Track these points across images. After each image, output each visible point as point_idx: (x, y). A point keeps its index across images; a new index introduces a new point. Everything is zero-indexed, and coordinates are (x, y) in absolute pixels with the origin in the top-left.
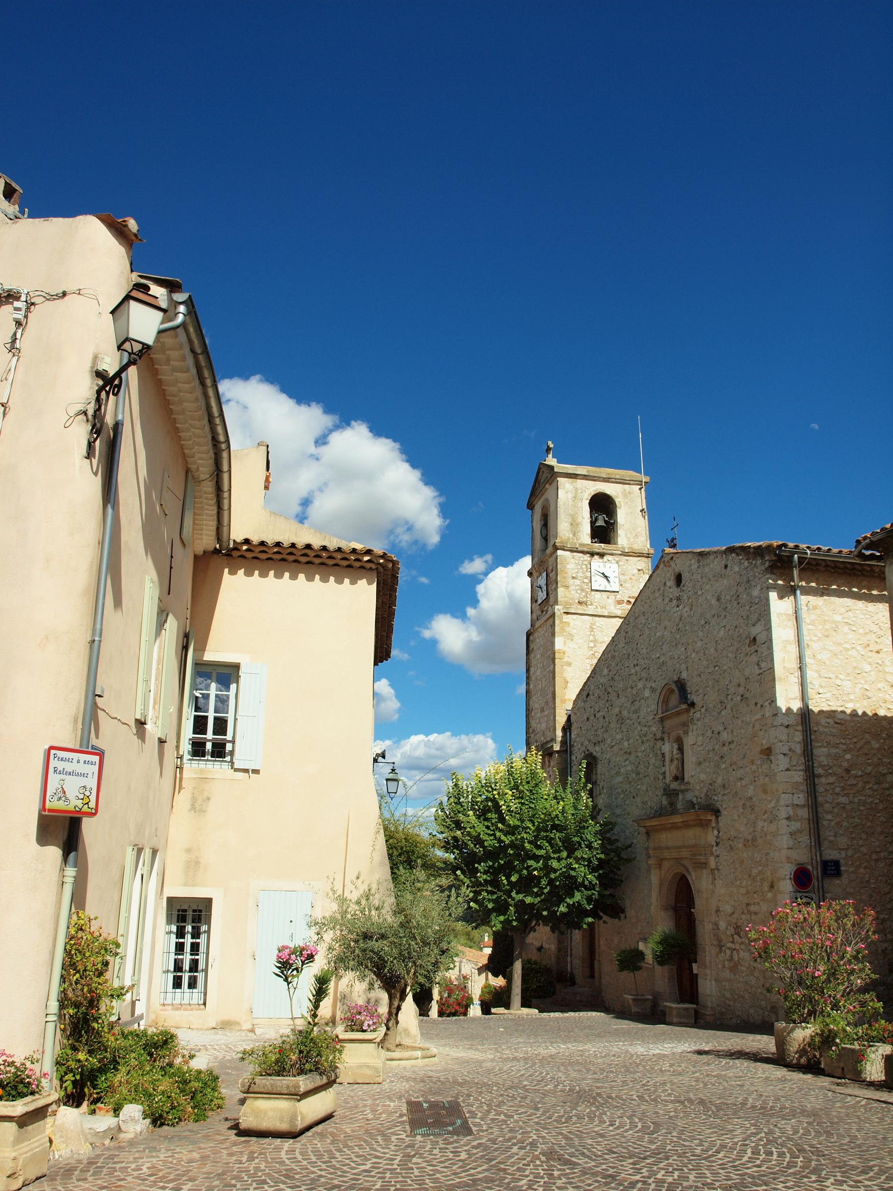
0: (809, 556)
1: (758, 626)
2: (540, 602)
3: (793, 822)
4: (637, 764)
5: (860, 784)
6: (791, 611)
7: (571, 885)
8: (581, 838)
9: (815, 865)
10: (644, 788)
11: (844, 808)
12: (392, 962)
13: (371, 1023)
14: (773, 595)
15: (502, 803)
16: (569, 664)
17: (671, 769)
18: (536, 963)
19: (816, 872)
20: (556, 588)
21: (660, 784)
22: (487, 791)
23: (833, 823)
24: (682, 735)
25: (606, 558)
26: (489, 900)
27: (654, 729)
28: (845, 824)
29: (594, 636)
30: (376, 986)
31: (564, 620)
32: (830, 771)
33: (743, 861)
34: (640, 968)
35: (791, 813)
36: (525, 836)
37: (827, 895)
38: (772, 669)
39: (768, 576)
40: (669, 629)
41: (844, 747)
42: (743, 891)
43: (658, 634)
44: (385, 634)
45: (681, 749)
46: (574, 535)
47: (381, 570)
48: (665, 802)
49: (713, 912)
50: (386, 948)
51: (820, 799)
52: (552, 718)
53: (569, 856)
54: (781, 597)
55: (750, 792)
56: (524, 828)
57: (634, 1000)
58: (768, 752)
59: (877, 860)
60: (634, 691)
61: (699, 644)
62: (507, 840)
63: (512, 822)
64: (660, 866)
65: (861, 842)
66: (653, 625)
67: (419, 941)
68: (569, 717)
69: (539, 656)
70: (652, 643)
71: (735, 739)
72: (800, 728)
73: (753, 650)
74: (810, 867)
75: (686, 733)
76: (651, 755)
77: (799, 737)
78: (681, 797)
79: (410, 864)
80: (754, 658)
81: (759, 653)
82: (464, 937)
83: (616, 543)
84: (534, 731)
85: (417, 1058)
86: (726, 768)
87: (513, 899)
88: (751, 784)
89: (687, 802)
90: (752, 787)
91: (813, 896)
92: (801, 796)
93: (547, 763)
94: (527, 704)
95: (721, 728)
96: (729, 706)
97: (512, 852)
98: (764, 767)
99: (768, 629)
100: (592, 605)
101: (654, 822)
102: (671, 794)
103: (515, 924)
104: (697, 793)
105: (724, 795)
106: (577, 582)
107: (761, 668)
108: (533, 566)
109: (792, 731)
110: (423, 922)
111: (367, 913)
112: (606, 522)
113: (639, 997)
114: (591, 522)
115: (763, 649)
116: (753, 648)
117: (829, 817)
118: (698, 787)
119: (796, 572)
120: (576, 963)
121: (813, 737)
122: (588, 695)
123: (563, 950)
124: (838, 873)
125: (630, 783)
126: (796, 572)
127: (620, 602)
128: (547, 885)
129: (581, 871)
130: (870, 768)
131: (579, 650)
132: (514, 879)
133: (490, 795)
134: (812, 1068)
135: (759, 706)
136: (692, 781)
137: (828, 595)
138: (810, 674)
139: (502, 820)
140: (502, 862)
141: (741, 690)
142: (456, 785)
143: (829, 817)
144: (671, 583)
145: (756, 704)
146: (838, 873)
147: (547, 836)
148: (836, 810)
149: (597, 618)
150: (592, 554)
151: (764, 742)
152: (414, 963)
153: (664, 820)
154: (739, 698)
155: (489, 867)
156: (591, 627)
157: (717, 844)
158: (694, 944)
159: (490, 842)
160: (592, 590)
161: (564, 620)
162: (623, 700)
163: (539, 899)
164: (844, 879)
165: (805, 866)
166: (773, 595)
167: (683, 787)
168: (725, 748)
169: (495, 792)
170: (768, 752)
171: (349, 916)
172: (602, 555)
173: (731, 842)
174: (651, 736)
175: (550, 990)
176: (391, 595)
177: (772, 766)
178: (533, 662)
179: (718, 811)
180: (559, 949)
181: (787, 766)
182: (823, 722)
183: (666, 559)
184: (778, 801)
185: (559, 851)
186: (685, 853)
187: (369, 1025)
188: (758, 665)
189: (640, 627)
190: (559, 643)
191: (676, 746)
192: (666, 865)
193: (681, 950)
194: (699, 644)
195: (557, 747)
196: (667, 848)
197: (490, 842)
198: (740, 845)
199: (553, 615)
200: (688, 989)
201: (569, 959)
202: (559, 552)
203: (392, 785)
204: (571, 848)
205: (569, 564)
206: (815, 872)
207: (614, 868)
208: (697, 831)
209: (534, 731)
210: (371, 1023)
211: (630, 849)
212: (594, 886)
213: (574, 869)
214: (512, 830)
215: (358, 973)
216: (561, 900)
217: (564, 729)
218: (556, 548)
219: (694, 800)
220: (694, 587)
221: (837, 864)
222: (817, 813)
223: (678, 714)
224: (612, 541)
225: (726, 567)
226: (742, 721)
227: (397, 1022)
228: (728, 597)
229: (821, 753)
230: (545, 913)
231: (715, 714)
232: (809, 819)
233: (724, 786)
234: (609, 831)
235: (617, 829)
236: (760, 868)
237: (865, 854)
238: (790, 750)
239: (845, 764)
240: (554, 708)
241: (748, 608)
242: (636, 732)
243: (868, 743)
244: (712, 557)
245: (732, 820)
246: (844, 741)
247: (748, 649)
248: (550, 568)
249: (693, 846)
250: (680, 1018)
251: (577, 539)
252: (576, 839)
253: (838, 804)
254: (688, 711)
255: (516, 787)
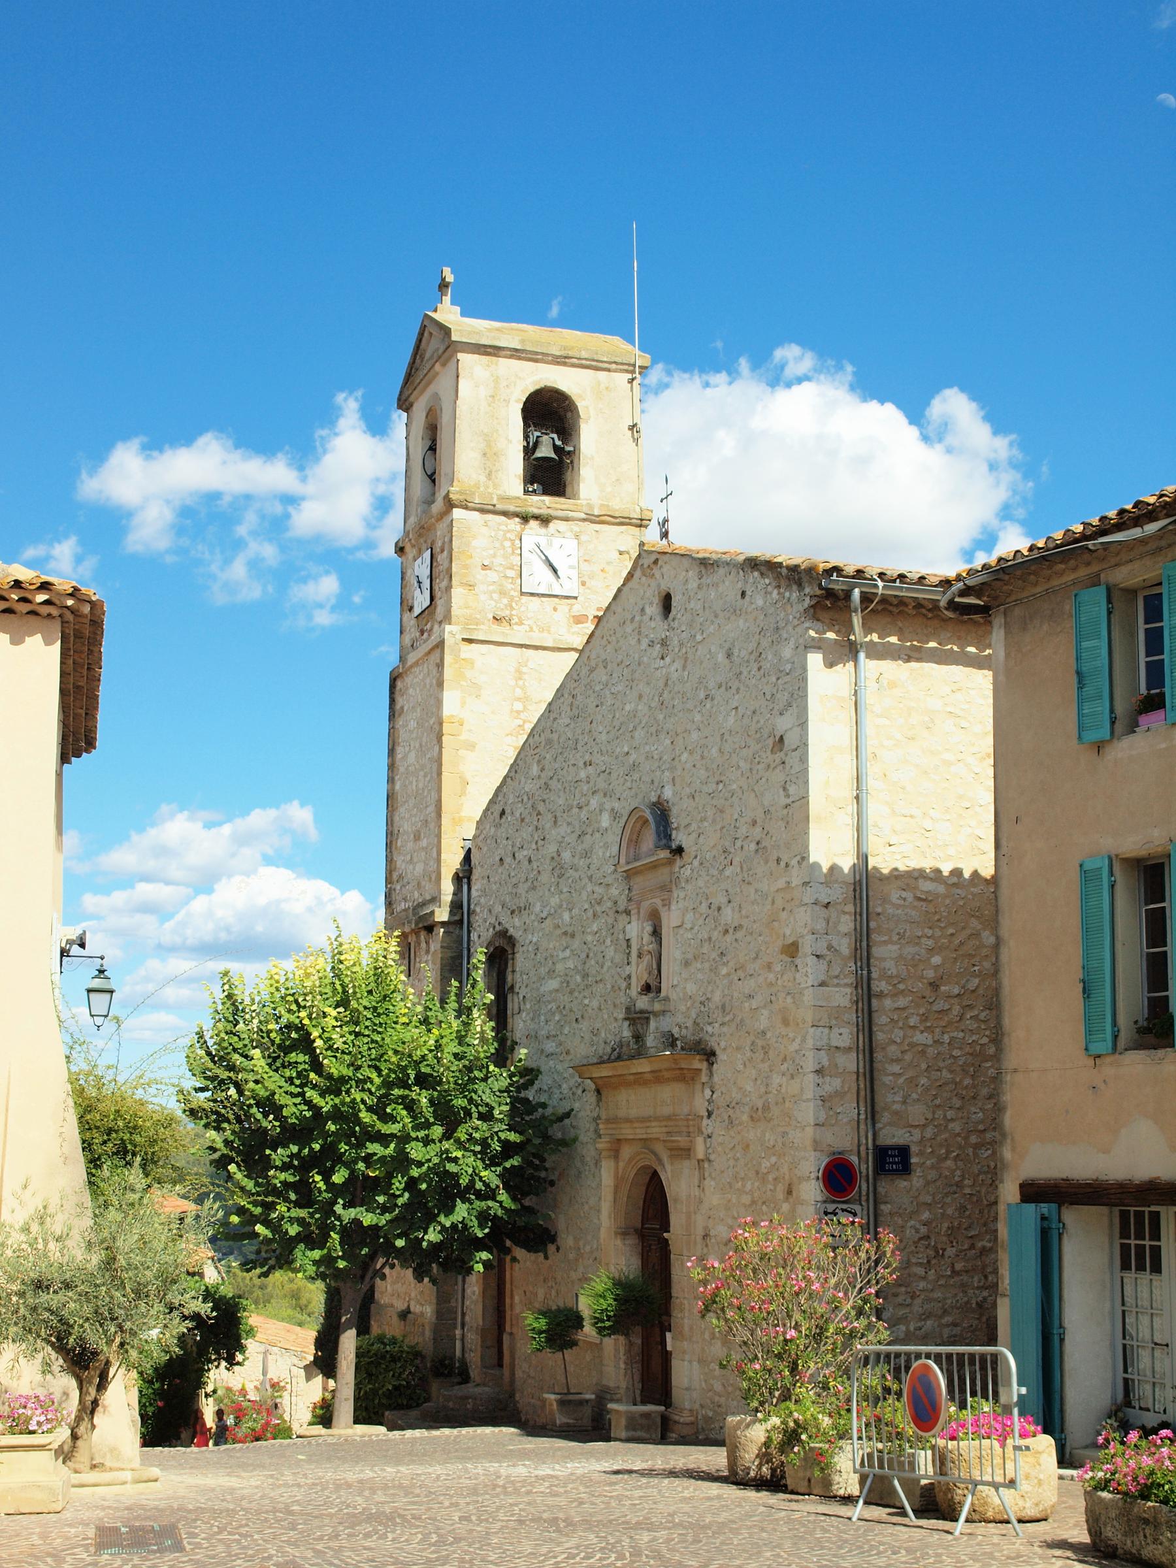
0: (880, 591)
1: (788, 714)
2: (417, 610)
3: (828, 1079)
4: (583, 956)
5: (956, 1010)
6: (846, 691)
7: (448, 1190)
8: (471, 1101)
9: (863, 1154)
10: (595, 1004)
11: (923, 1052)
12: (82, 1326)
13: (43, 1418)
14: (815, 660)
15: (315, 1034)
16: (471, 746)
17: (639, 972)
18: (394, 1341)
19: (864, 1166)
20: (449, 588)
21: (623, 999)
22: (289, 1011)
23: (901, 1080)
24: (660, 908)
25: (554, 525)
26: (291, 1220)
27: (614, 892)
28: (923, 1081)
29: (523, 688)
30: (56, 1368)
31: (463, 656)
32: (901, 986)
33: (748, 1146)
34: (573, 1344)
35: (825, 1062)
36: (358, 1096)
37: (883, 1207)
38: (804, 798)
39: (807, 624)
40: (645, 700)
41: (930, 943)
42: (746, 1199)
43: (628, 707)
44: (83, 712)
45: (656, 933)
46: (489, 476)
47: (69, 617)
48: (627, 1034)
49: (699, 1239)
50: (72, 1305)
51: (880, 1037)
52: (435, 855)
53: (447, 1136)
54: (830, 664)
55: (763, 1022)
56: (358, 1082)
57: (562, 1403)
58: (792, 950)
59: (977, 1147)
60: (584, 815)
61: (695, 735)
62: (326, 1104)
63: (334, 1067)
64: (615, 1154)
65: (950, 1114)
66: (620, 688)
67: (128, 1290)
68: (467, 858)
69: (413, 724)
70: (617, 723)
71: (744, 922)
72: (850, 908)
73: (778, 761)
74: (854, 1159)
75: (667, 903)
76: (608, 942)
77: (847, 924)
78: (653, 1024)
79: (123, 1152)
80: (778, 776)
81: (788, 766)
82: (285, 1302)
83: (575, 496)
84: (401, 877)
85: (124, 1483)
86: (728, 974)
87: (339, 1218)
88: (765, 1007)
89: (663, 1034)
90: (765, 1012)
91: (857, 1208)
92: (845, 1031)
93: (423, 945)
94: (390, 822)
95: (724, 900)
96: (736, 861)
97: (333, 1128)
98: (785, 977)
99: (803, 724)
100: (521, 623)
101: (605, 1071)
102: (638, 1019)
103: (341, 1264)
104: (680, 1019)
105: (723, 1024)
106: (492, 576)
107: (788, 796)
108: (406, 533)
109: (834, 915)
110: (137, 1259)
111: (40, 1246)
112: (556, 449)
113: (571, 1397)
114: (526, 449)
115: (793, 760)
116: (779, 756)
117: (896, 1068)
118: (683, 1008)
119: (857, 620)
120: (469, 1343)
121: (873, 924)
122: (503, 813)
123: (446, 1315)
124: (905, 1168)
125: (571, 993)
126: (857, 620)
127: (579, 619)
128: (404, 1190)
129: (467, 1165)
130: (977, 981)
131: (490, 714)
132: (338, 1178)
133: (292, 1018)
134: (774, 1484)
135: (783, 864)
136: (673, 996)
137: (919, 660)
138: (874, 809)
139: (317, 1066)
140: (317, 1147)
141: (757, 832)
142: (229, 997)
143: (896, 1068)
144: (654, 609)
145: (778, 860)
146: (905, 1168)
147: (404, 1097)
148: (908, 1057)
149: (531, 652)
150: (525, 519)
151: (788, 932)
152: (120, 1327)
153: (621, 1068)
154: (753, 846)
155: (292, 1156)
156: (519, 671)
157: (710, 1115)
158: (668, 1297)
159: (292, 1109)
160: (522, 593)
161: (463, 656)
162: (563, 829)
163: (388, 1216)
164: (917, 1179)
165: (846, 1156)
166: (815, 660)
167: (657, 1007)
168: (729, 938)
169: (303, 1014)
170: (792, 950)
171: (9, 1253)
172: (545, 520)
173: (731, 1112)
174: (609, 904)
175: (402, 1388)
176: (90, 652)
177: (798, 975)
178: (402, 735)
179: (713, 1054)
180: (439, 1314)
181: (822, 977)
182: (894, 896)
183: (647, 561)
184: (804, 1040)
185: (427, 1125)
186: (656, 1130)
187: (39, 1424)
188: (785, 789)
189: (597, 688)
190: (452, 703)
191: (649, 928)
192: (626, 1152)
193: (645, 1308)
194: (695, 735)
195: (442, 914)
196: (628, 1120)
197: (292, 1109)
198: (745, 1118)
199: (440, 645)
200: (655, 1380)
201: (458, 1332)
202: (457, 513)
203: (100, 1000)
204: (450, 1119)
205: (475, 537)
206: (863, 1167)
207: (537, 1153)
208: (678, 1089)
209: (401, 877)
210: (43, 1418)
211: (567, 1121)
212: (493, 1191)
213: (455, 1160)
214: (335, 1086)
215: (24, 1346)
216: (431, 1218)
217: (458, 879)
218: (450, 505)
219: (676, 1031)
220: (690, 625)
221: (904, 1152)
222: (872, 1061)
223: (654, 866)
224: (568, 490)
225: (743, 594)
226: (756, 891)
227: (93, 1427)
228: (744, 653)
229: (886, 953)
230: (400, 1243)
231: (715, 873)
232: (858, 1073)
233: (723, 1007)
234: (525, 1086)
235: (544, 1081)
236: (773, 1159)
237: (958, 1135)
238: (830, 947)
239: (930, 974)
240: (439, 836)
241: (774, 679)
242: (584, 895)
243: (976, 935)
244: (722, 571)
245: (734, 1073)
246: (930, 933)
247: (771, 757)
248: (440, 544)
249: (669, 1118)
250: (634, 1430)
251: (496, 486)
252: (460, 1102)
253: (912, 1045)
254: (670, 862)
255: (344, 1003)
